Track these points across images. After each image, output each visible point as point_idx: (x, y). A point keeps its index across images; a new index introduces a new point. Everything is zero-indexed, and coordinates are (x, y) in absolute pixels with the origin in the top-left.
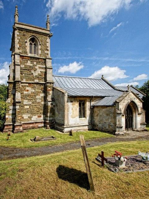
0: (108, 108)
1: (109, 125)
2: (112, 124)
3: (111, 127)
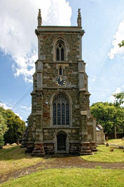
0: (98, 132)
1: (99, 141)
2: (101, 140)
3: (100, 142)
